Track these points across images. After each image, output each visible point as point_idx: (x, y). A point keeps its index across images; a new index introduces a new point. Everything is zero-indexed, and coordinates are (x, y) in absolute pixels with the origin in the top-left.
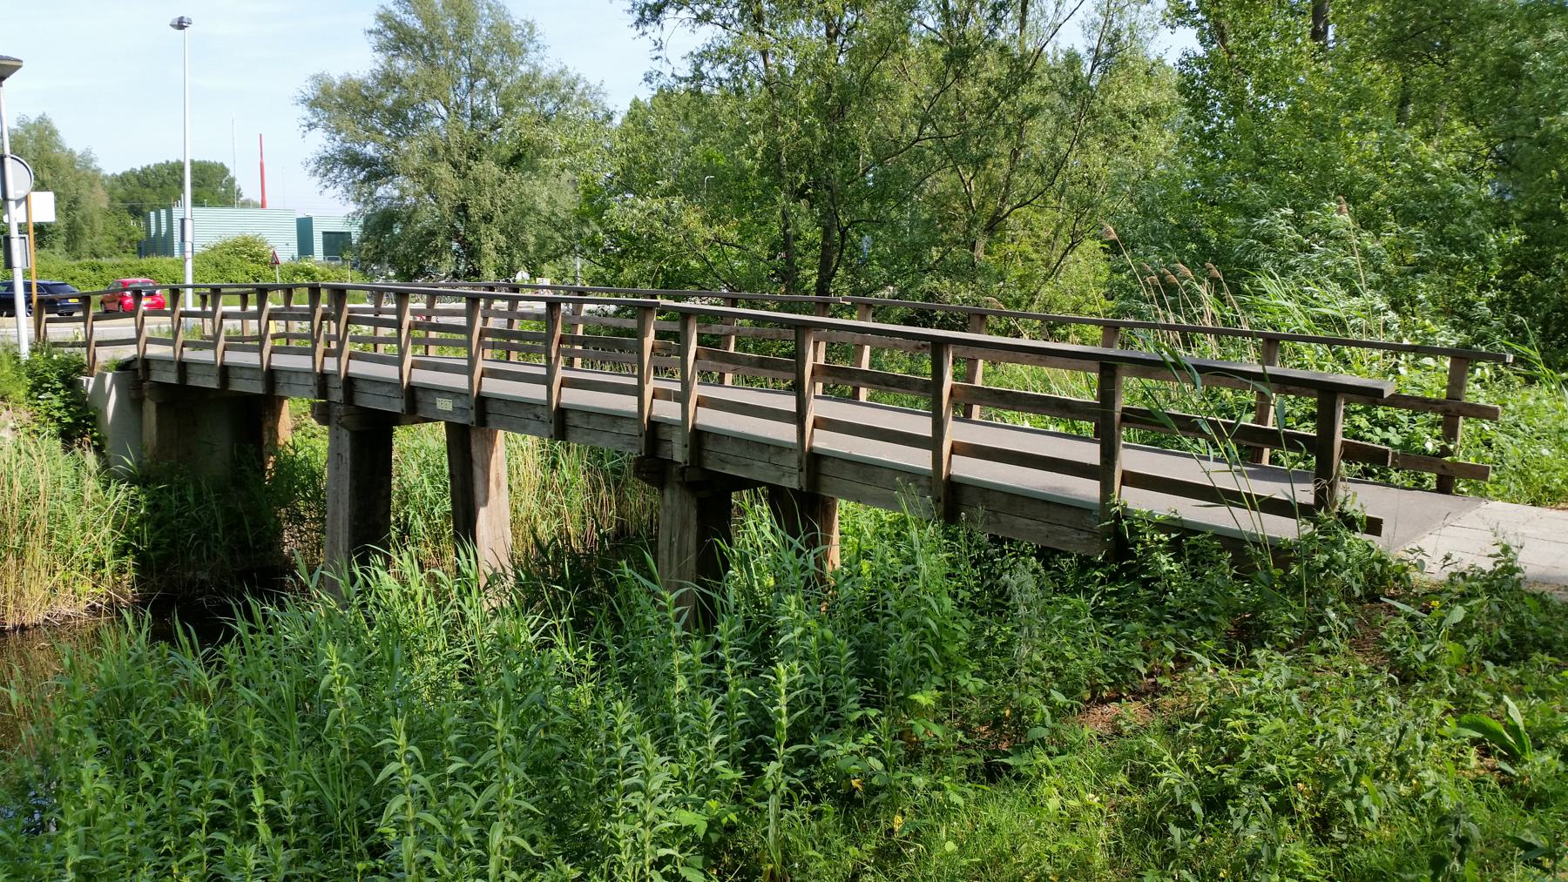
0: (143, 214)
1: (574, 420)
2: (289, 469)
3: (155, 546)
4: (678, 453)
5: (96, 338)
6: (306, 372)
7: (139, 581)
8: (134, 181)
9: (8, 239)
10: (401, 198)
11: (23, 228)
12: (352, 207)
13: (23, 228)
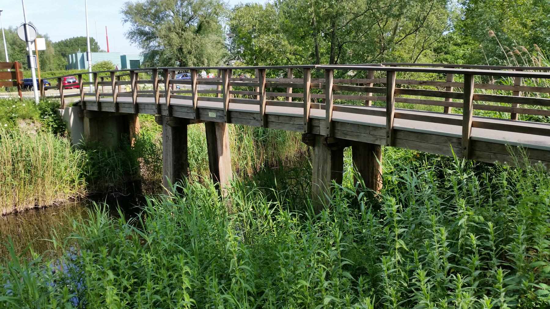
0: (66, 56)
1: (271, 119)
2: (141, 144)
3: (93, 174)
4: (323, 131)
5: (64, 94)
6: (152, 104)
7: (88, 187)
8: (62, 45)
9: (29, 57)
10: (159, 46)
11: (34, 53)
12: (142, 50)
13: (34, 53)
